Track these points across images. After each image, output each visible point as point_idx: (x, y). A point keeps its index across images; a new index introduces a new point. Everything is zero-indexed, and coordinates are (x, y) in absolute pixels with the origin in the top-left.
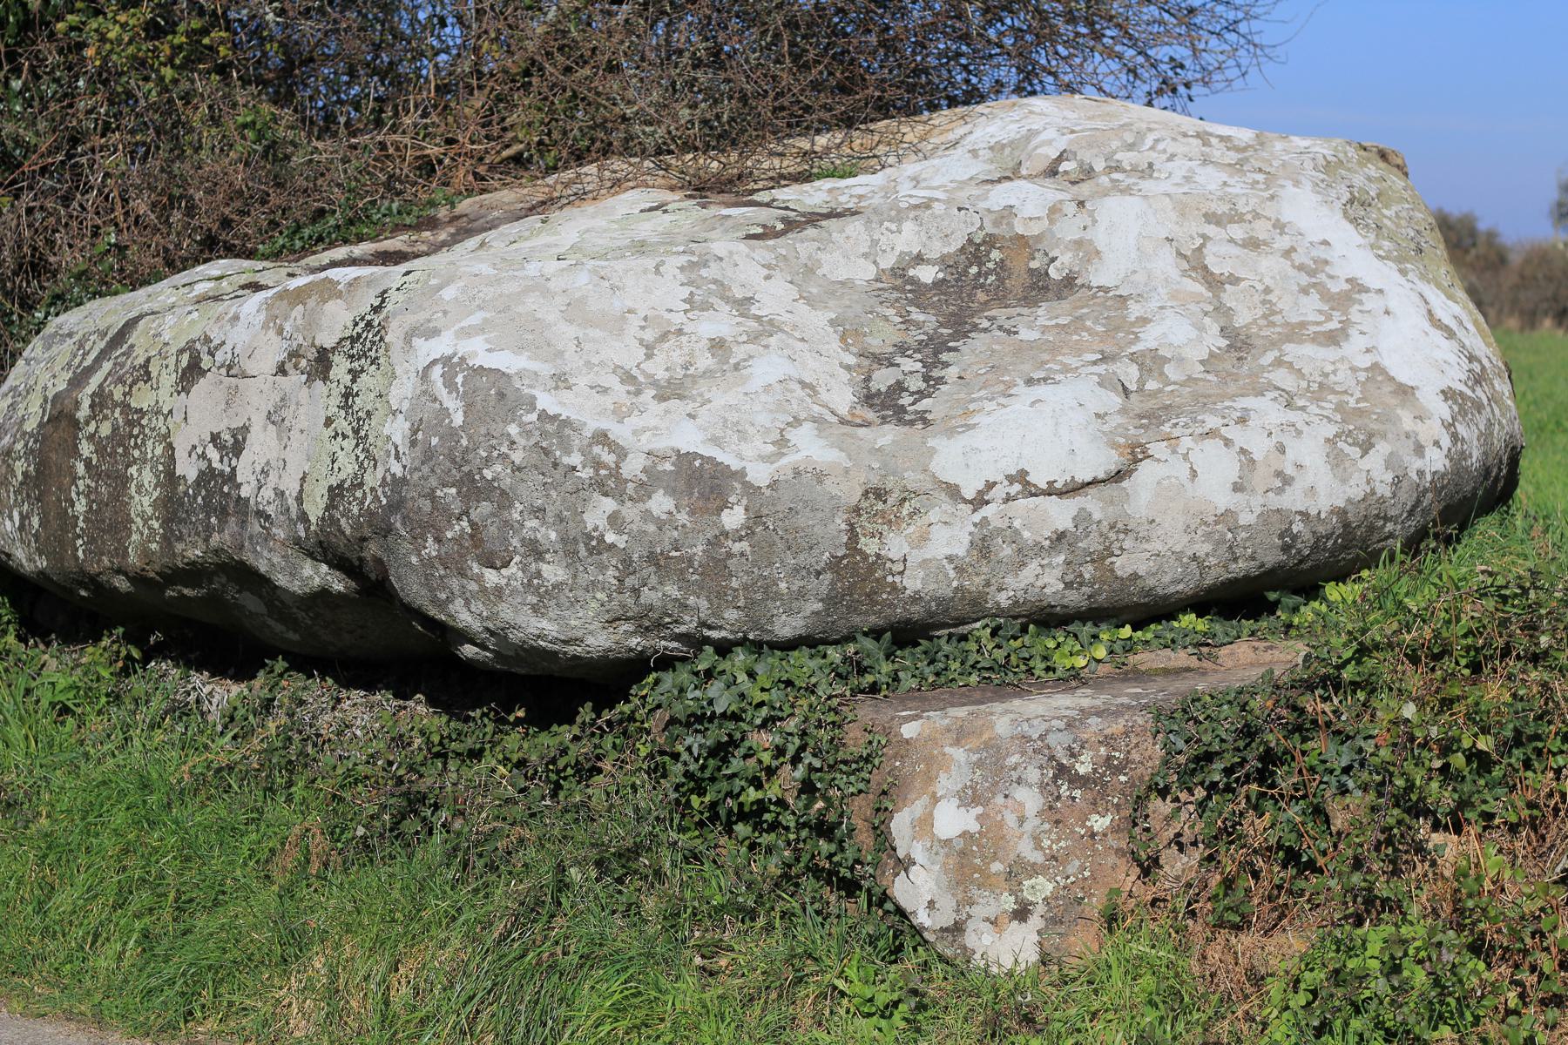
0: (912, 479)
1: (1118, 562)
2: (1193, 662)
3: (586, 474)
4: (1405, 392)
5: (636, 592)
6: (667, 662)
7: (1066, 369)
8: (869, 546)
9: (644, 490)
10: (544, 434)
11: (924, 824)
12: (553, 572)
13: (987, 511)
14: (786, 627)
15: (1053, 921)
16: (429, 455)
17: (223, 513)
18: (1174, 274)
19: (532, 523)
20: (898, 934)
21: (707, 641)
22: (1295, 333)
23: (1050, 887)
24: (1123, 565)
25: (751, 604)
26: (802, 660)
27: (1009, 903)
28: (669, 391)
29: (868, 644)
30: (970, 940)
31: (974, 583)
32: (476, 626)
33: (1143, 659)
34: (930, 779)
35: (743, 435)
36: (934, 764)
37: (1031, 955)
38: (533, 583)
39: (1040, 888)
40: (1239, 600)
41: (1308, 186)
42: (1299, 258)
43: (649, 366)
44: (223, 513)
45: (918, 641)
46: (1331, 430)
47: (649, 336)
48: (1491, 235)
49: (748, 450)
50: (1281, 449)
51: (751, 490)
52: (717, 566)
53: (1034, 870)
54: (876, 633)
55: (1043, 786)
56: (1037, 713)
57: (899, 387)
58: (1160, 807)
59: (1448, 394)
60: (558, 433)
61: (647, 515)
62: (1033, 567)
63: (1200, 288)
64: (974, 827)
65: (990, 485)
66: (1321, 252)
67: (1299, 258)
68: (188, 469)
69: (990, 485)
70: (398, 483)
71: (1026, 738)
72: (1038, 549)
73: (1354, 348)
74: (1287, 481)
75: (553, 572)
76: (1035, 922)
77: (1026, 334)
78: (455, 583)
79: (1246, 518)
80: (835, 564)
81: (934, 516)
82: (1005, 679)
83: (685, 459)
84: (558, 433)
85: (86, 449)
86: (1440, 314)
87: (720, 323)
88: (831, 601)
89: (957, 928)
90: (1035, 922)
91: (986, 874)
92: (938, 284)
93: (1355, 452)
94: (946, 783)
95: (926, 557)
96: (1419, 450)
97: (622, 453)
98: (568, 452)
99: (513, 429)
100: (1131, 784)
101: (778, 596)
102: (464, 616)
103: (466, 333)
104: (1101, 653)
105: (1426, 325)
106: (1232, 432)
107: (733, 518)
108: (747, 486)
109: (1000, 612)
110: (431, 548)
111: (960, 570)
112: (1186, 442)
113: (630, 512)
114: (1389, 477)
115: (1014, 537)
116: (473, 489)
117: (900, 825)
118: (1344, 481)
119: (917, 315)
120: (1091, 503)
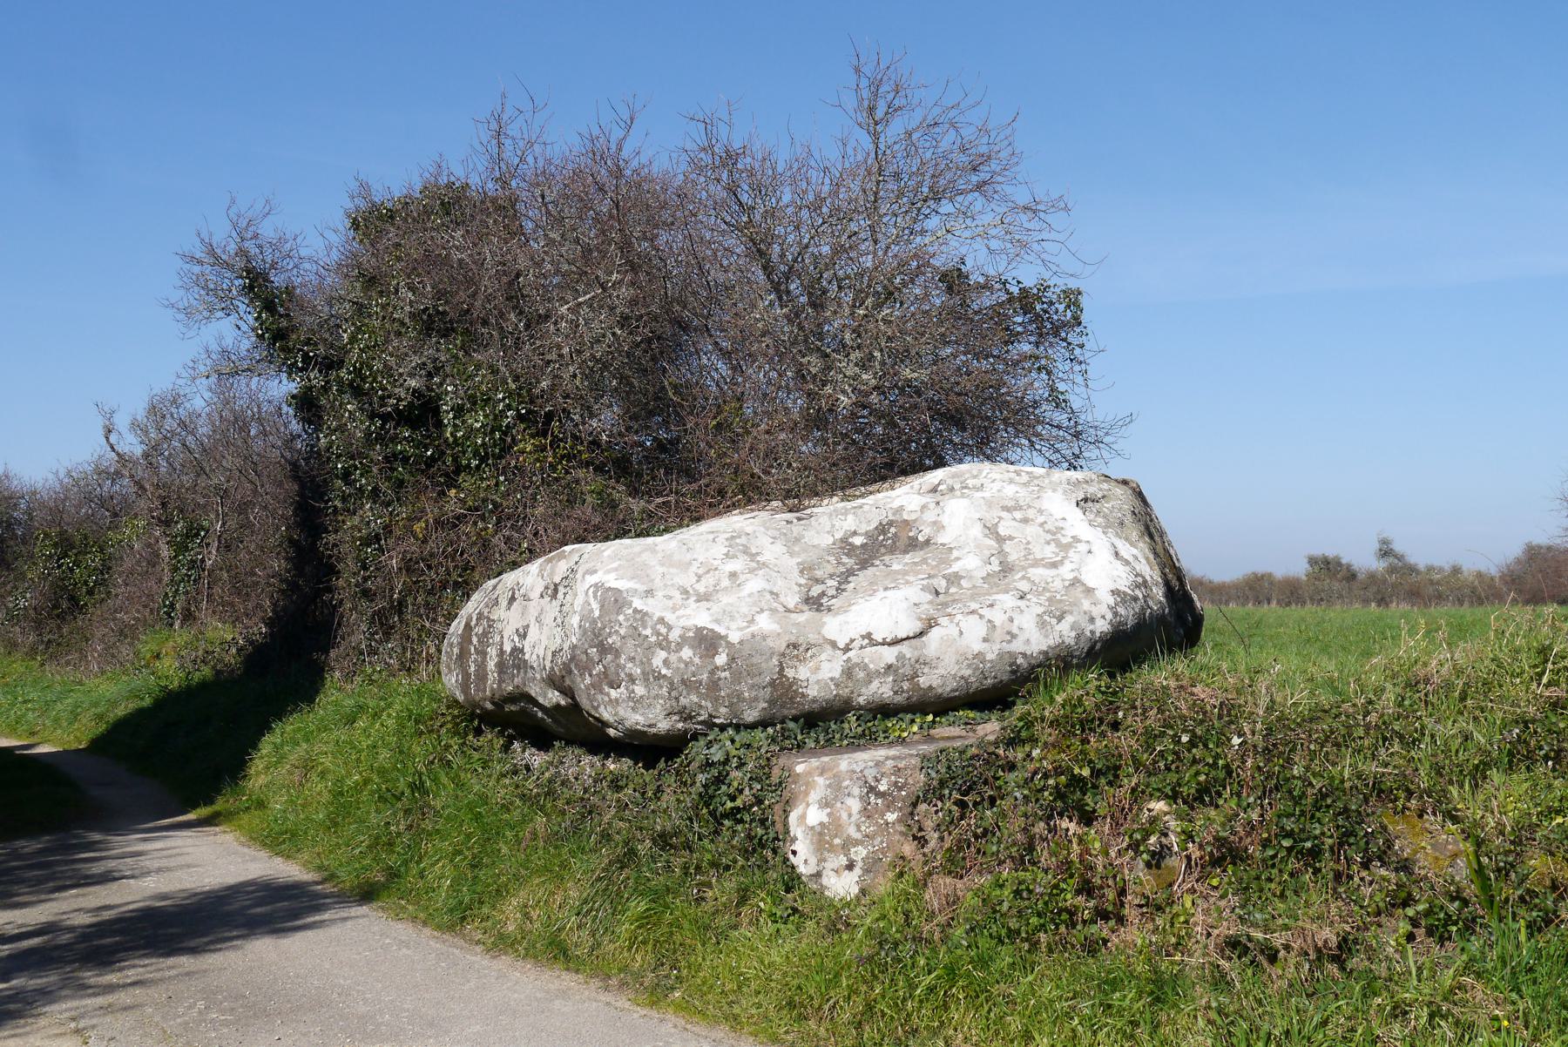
0: (812, 638)
1: (921, 680)
2: (964, 733)
3: (653, 639)
4: (1089, 591)
5: (677, 699)
6: (695, 737)
7: (907, 582)
8: (790, 673)
9: (679, 646)
10: (635, 620)
11: (803, 817)
12: (640, 690)
13: (850, 654)
14: (750, 716)
15: (867, 871)
16: (585, 633)
17: (519, 669)
18: (980, 536)
19: (630, 665)
20: (792, 881)
21: (715, 725)
22: (1037, 563)
23: (865, 852)
24: (923, 681)
25: (731, 705)
26: (759, 734)
27: (844, 861)
28: (703, 598)
29: (791, 725)
30: (825, 881)
31: (845, 692)
32: (612, 720)
33: (938, 732)
34: (807, 794)
35: (732, 618)
36: (810, 785)
37: (855, 890)
38: (631, 697)
39: (859, 853)
40: (990, 697)
41: (1060, 491)
42: (1047, 527)
43: (697, 586)
44: (519, 669)
45: (821, 722)
46: (1040, 610)
47: (700, 572)
48: (1349, 566)
49: (734, 626)
50: (1011, 620)
51: (730, 645)
52: (714, 685)
53: (857, 843)
54: (795, 719)
55: (861, 798)
56: (863, 760)
57: (823, 594)
58: (923, 807)
59: (1114, 592)
60: (642, 619)
61: (680, 660)
62: (875, 684)
63: (993, 543)
64: (826, 820)
65: (852, 641)
66: (1060, 524)
67: (1047, 527)
68: (508, 648)
69: (852, 641)
70: (574, 647)
71: (854, 772)
72: (878, 673)
73: (1066, 571)
74: (1014, 636)
75: (640, 690)
76: (857, 871)
77: (895, 567)
78: (599, 697)
79: (990, 657)
80: (772, 683)
81: (823, 657)
82: (867, 739)
83: (699, 630)
84: (642, 619)
85: (475, 640)
86: (1123, 553)
87: (736, 565)
88: (772, 702)
89: (818, 875)
90: (857, 871)
91: (831, 845)
92: (863, 546)
93: (1054, 621)
94: (814, 796)
95: (818, 678)
96: (1092, 620)
97: (670, 628)
98: (645, 628)
99: (621, 618)
100: (908, 795)
101: (744, 700)
102: (606, 714)
103: (608, 572)
104: (915, 728)
105: (1112, 558)
106: (985, 612)
107: (721, 660)
108: (728, 643)
109: (861, 708)
110: (588, 680)
111: (837, 685)
112: (959, 617)
113: (673, 658)
114: (1073, 634)
115: (865, 668)
116: (604, 649)
117: (793, 818)
118: (1046, 636)
119: (845, 559)
120: (904, 648)
